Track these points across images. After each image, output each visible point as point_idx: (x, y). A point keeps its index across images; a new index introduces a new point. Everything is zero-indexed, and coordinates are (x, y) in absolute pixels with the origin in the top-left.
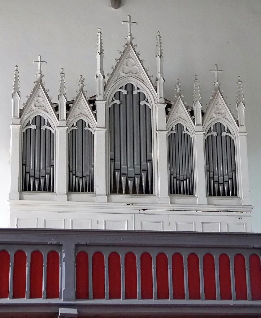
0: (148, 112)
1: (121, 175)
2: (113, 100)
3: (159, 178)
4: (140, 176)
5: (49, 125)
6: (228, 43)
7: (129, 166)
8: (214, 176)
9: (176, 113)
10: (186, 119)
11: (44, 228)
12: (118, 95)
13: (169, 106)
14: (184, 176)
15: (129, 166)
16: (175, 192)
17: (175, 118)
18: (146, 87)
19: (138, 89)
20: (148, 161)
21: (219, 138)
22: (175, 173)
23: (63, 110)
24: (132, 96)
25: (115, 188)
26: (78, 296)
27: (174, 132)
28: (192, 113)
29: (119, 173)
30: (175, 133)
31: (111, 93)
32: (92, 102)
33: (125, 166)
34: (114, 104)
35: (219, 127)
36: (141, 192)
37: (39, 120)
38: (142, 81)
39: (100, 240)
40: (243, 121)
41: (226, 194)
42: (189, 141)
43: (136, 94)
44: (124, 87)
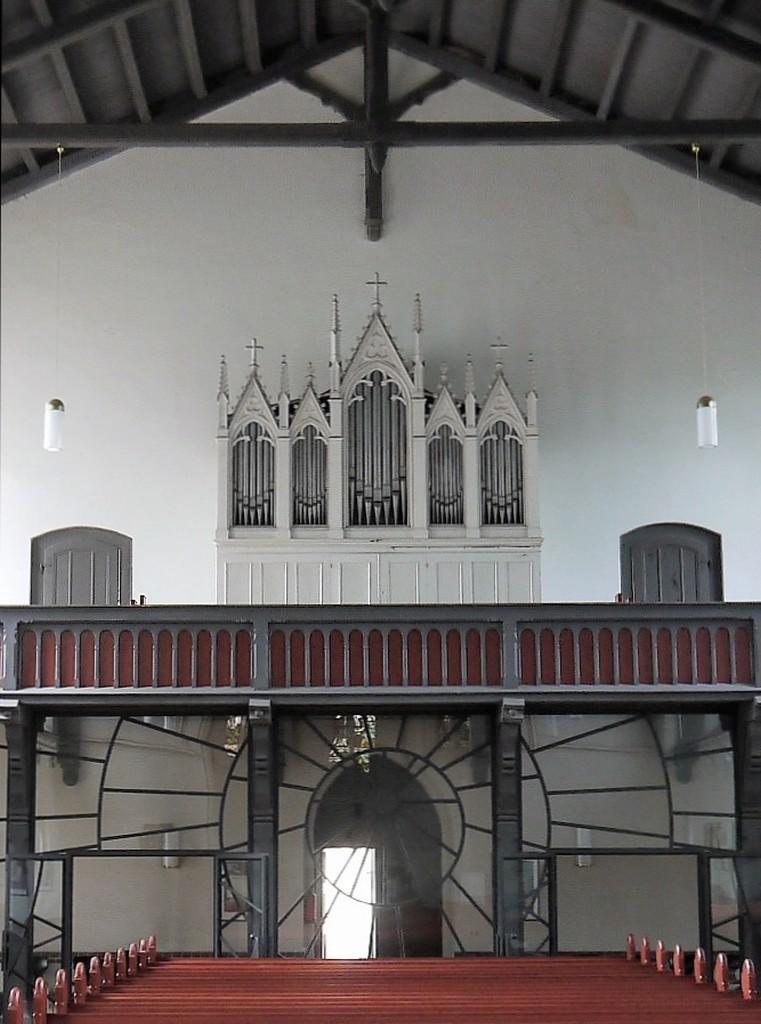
0: (401, 408)
16: (387, 520)
19: (389, 378)
34: (356, 402)
41: (252, 521)
44: (368, 377)
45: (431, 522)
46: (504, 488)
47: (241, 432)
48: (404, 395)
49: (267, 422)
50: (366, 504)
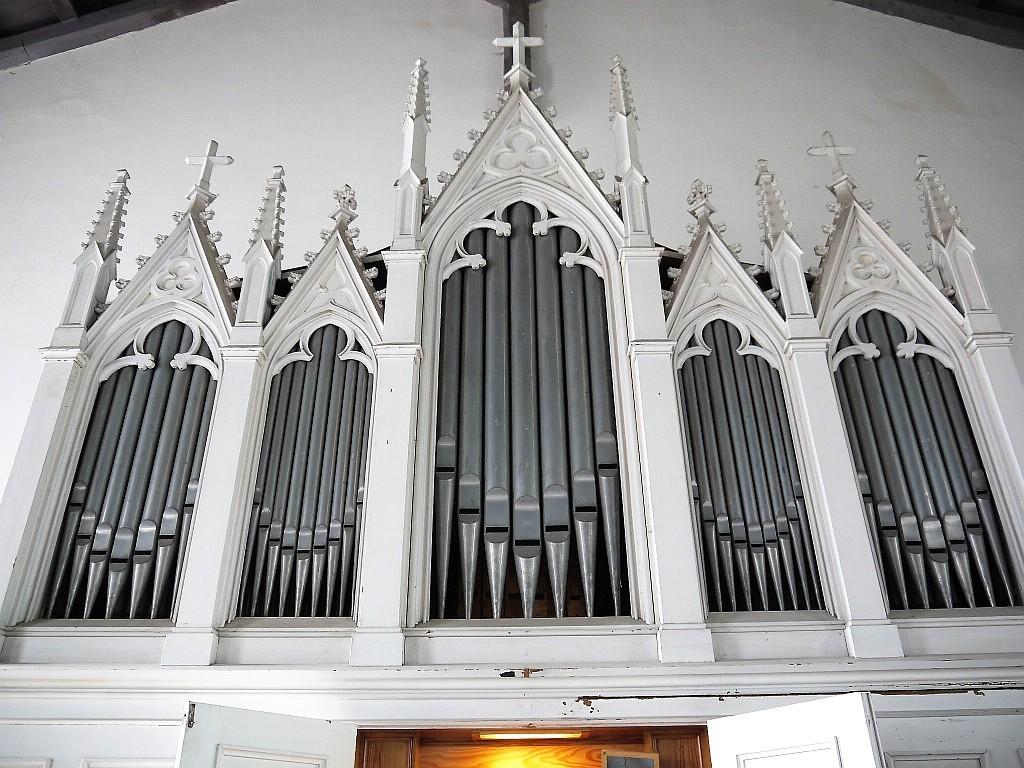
0: (590, 286)
1: (461, 516)
2: (457, 256)
3: (652, 537)
4: (566, 534)
5: (206, 353)
6: (816, 187)
8: (898, 521)
9: (700, 283)
10: (745, 300)
12: (479, 239)
14: (765, 526)
15: (518, 495)
16: (733, 600)
17: (701, 302)
18: (578, 204)
19: (551, 215)
20: (600, 471)
21: (887, 365)
22: (722, 514)
23: (254, 301)
24: (528, 241)
27: (702, 350)
29: (475, 526)
30: (708, 354)
31: (450, 230)
33: (499, 493)
34: (463, 271)
38: (567, 190)
40: (974, 290)
41: (970, 596)
42: (766, 382)
43: (544, 231)
44: (499, 214)
45: (712, 606)
46: (977, 485)
47: (297, 345)
48: (593, 251)
49: (206, 319)
50: (491, 548)
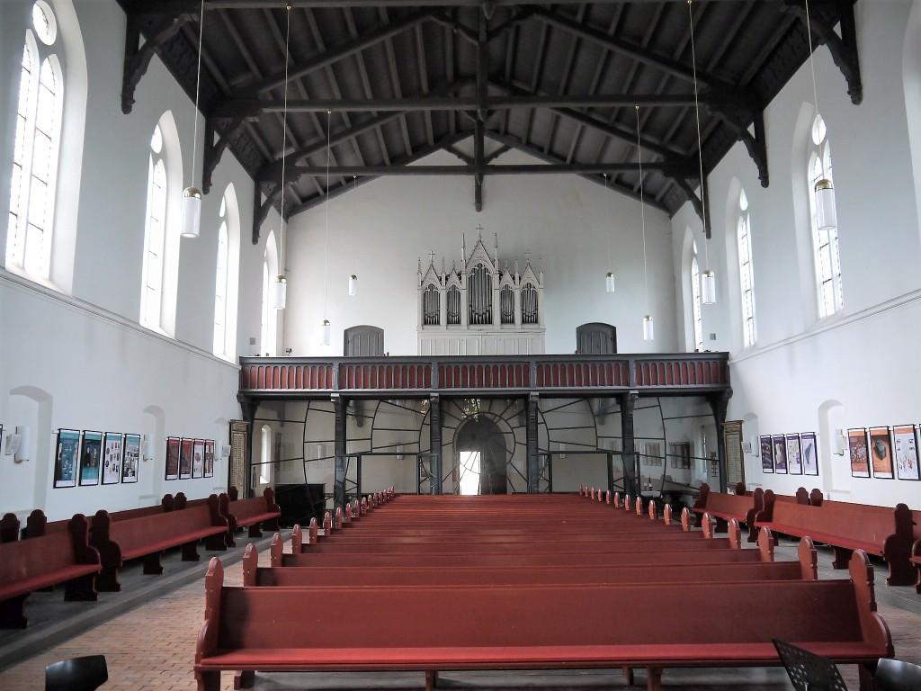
7: (480, 310)
11: (415, 353)
13: (501, 275)
25: (472, 321)
26: (440, 387)
28: (514, 278)
31: (469, 269)
32: (459, 275)
35: (529, 285)
36: (486, 323)
37: (431, 286)
39: (450, 360)
